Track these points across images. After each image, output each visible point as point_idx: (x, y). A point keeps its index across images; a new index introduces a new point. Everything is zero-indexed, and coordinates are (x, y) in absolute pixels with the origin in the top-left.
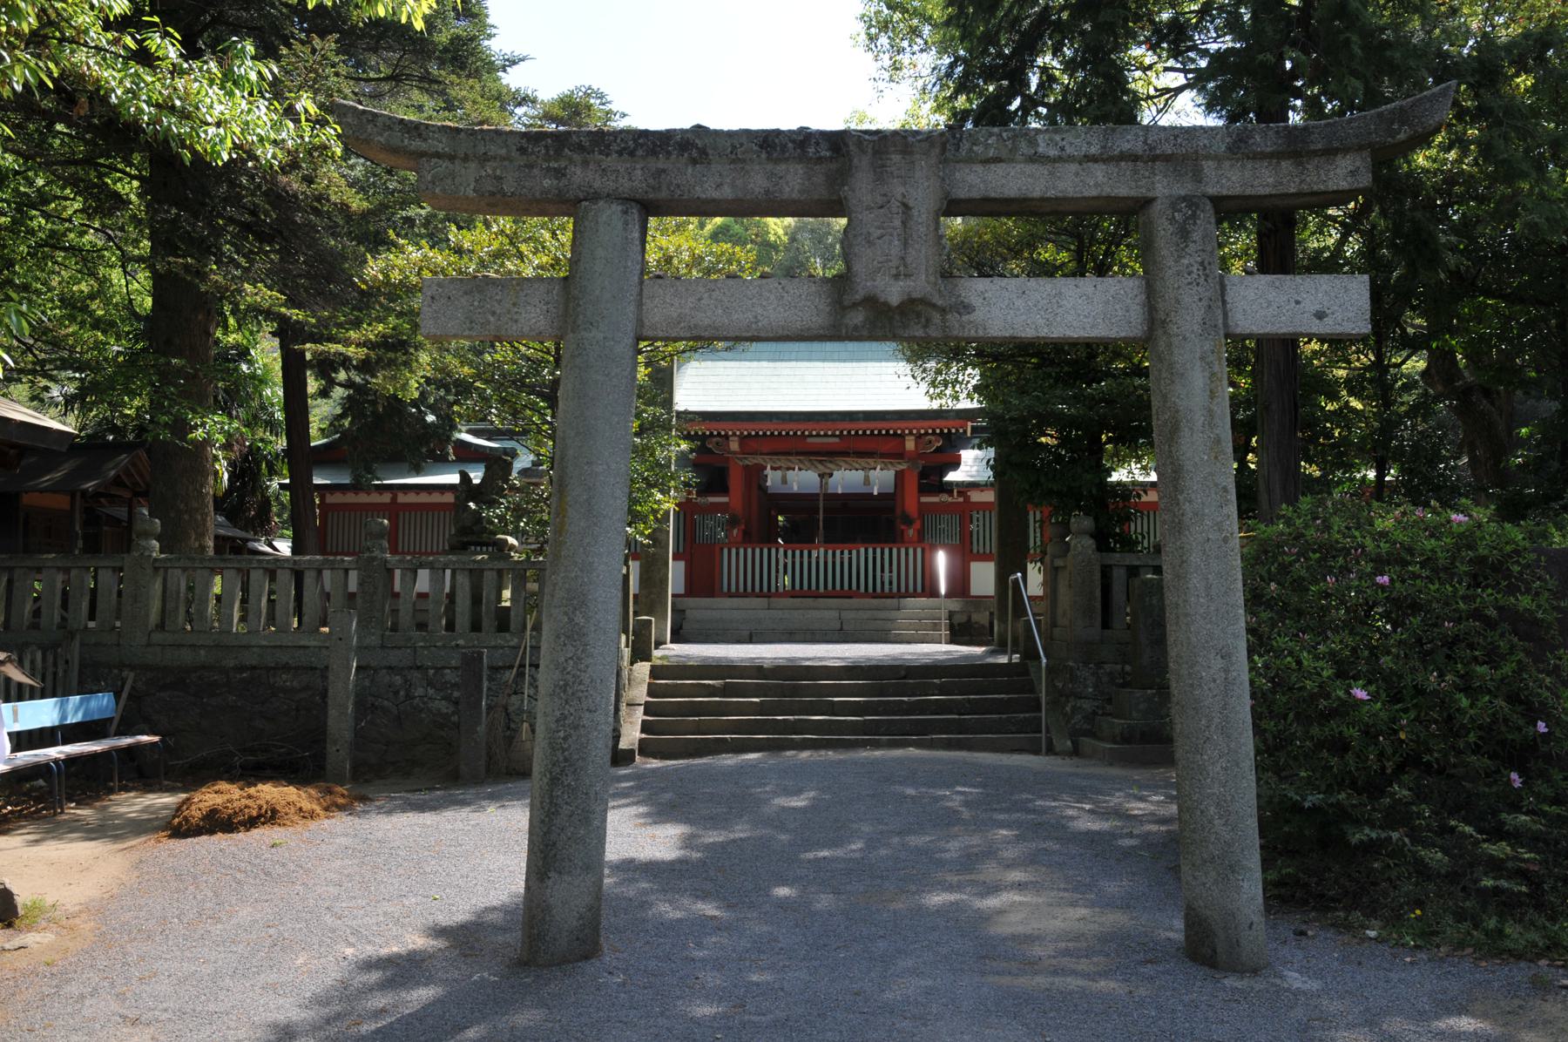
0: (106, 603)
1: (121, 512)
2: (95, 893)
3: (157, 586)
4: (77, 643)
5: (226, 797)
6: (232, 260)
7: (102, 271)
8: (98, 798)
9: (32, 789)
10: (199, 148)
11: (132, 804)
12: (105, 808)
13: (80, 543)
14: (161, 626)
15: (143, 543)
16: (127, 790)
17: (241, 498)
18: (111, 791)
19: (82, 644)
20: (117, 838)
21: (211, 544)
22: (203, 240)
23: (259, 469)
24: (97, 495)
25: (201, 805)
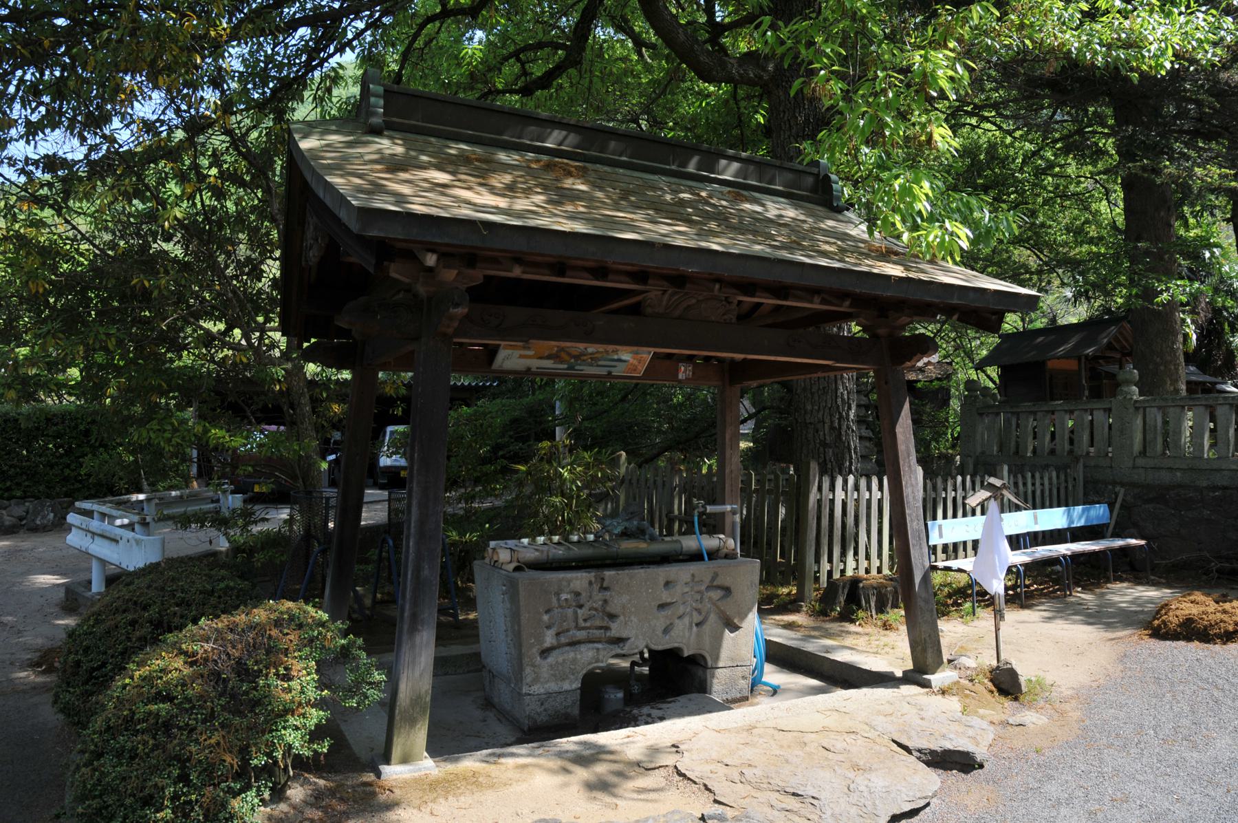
0: (1101, 434)
1: (1114, 368)
2: (1084, 679)
3: (1139, 421)
4: (1081, 465)
5: (1202, 609)
6: (1183, 155)
7: (1094, 206)
8: (1099, 585)
9: (1053, 572)
10: (1145, 67)
11: (1128, 594)
12: (1103, 595)
13: (1087, 393)
14: (1143, 453)
15: (1125, 389)
16: (1122, 581)
17: (1209, 352)
18: (1108, 581)
19: (1085, 467)
20: (1109, 626)
21: (1184, 387)
22: (1157, 144)
23: (1223, 329)
24: (1095, 358)
25: (1178, 613)
